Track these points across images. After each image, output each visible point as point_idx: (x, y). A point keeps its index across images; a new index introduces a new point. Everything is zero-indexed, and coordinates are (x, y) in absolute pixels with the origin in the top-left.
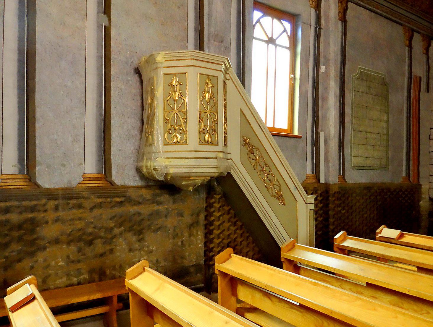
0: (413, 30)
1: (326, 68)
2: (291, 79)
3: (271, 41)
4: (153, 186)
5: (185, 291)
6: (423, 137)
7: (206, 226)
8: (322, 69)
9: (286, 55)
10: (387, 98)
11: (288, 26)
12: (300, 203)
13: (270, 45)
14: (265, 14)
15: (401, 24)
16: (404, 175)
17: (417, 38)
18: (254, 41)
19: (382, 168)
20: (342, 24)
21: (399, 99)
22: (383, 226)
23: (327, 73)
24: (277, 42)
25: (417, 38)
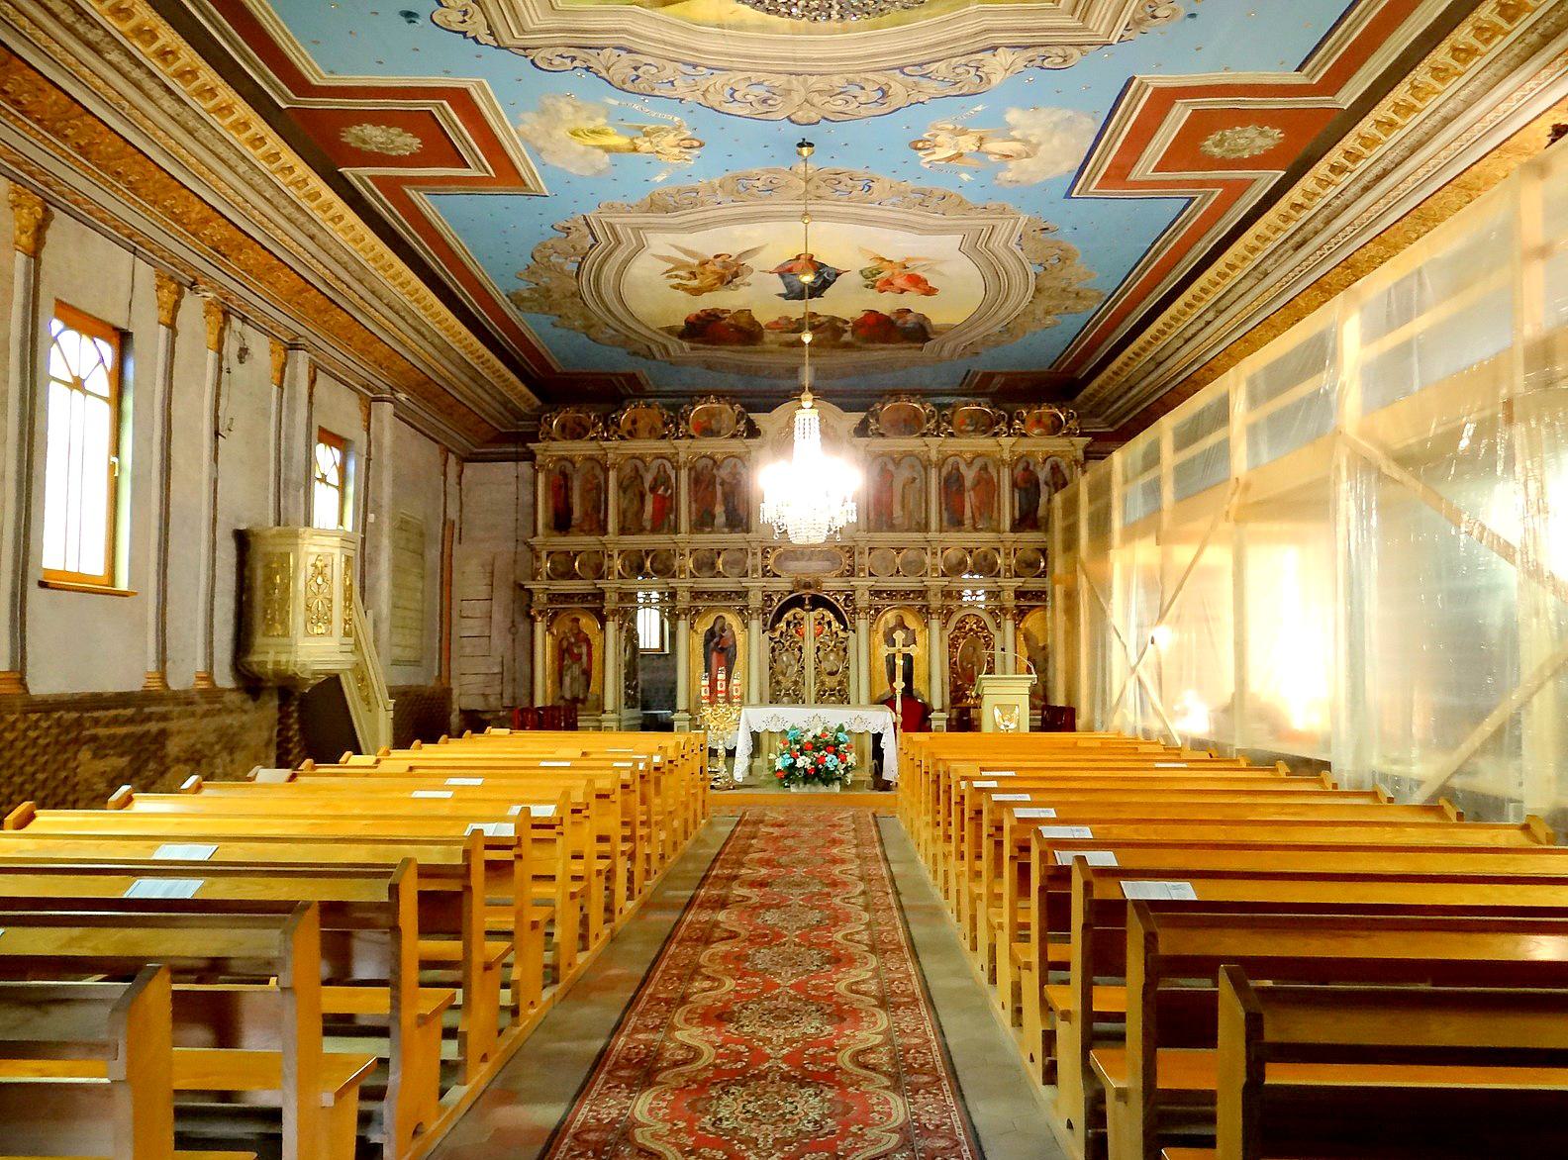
0: (448, 450)
1: (377, 517)
2: (112, 467)
3: (78, 384)
4: (230, 690)
5: (1093, 647)
6: (455, 614)
7: (279, 745)
8: (371, 517)
9: (105, 411)
10: (422, 555)
11: (337, 453)
12: (381, 709)
13: (75, 391)
14: (69, 325)
15: (437, 442)
16: (436, 674)
17: (452, 458)
18: (53, 384)
19: (416, 663)
20: (28, 263)
21: (433, 554)
22: (348, 753)
23: (377, 524)
24: (88, 386)
25: (452, 458)
